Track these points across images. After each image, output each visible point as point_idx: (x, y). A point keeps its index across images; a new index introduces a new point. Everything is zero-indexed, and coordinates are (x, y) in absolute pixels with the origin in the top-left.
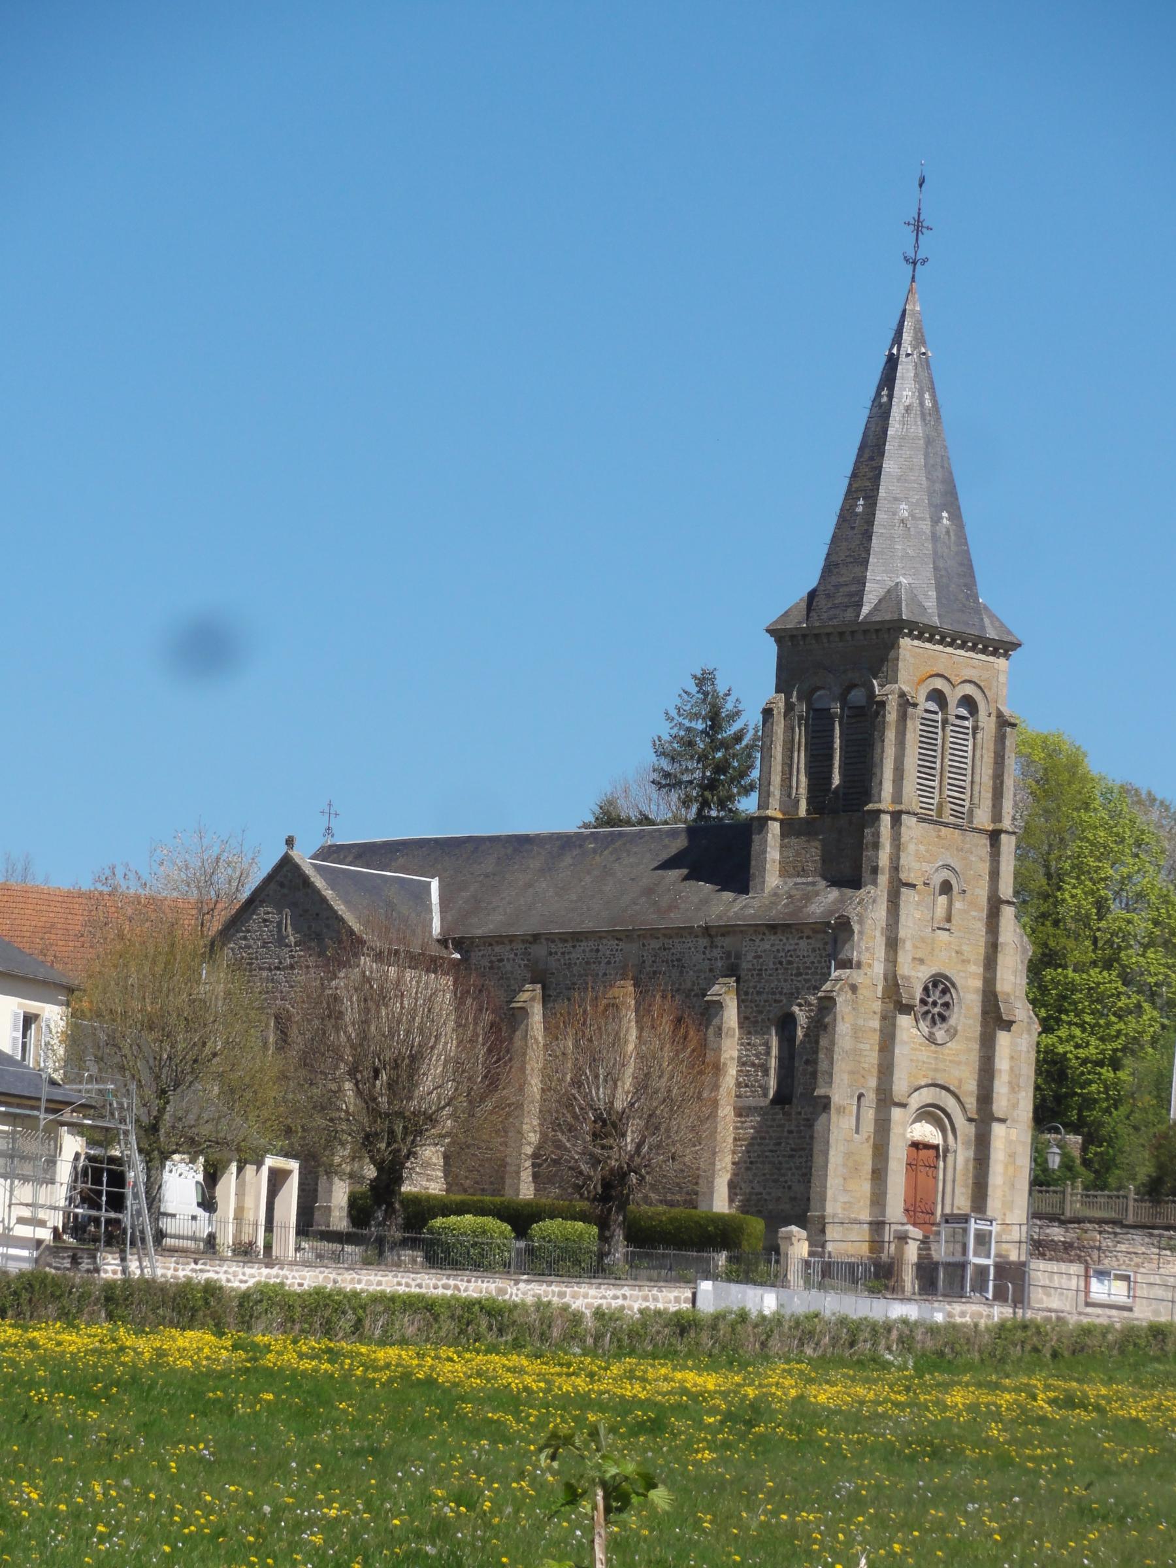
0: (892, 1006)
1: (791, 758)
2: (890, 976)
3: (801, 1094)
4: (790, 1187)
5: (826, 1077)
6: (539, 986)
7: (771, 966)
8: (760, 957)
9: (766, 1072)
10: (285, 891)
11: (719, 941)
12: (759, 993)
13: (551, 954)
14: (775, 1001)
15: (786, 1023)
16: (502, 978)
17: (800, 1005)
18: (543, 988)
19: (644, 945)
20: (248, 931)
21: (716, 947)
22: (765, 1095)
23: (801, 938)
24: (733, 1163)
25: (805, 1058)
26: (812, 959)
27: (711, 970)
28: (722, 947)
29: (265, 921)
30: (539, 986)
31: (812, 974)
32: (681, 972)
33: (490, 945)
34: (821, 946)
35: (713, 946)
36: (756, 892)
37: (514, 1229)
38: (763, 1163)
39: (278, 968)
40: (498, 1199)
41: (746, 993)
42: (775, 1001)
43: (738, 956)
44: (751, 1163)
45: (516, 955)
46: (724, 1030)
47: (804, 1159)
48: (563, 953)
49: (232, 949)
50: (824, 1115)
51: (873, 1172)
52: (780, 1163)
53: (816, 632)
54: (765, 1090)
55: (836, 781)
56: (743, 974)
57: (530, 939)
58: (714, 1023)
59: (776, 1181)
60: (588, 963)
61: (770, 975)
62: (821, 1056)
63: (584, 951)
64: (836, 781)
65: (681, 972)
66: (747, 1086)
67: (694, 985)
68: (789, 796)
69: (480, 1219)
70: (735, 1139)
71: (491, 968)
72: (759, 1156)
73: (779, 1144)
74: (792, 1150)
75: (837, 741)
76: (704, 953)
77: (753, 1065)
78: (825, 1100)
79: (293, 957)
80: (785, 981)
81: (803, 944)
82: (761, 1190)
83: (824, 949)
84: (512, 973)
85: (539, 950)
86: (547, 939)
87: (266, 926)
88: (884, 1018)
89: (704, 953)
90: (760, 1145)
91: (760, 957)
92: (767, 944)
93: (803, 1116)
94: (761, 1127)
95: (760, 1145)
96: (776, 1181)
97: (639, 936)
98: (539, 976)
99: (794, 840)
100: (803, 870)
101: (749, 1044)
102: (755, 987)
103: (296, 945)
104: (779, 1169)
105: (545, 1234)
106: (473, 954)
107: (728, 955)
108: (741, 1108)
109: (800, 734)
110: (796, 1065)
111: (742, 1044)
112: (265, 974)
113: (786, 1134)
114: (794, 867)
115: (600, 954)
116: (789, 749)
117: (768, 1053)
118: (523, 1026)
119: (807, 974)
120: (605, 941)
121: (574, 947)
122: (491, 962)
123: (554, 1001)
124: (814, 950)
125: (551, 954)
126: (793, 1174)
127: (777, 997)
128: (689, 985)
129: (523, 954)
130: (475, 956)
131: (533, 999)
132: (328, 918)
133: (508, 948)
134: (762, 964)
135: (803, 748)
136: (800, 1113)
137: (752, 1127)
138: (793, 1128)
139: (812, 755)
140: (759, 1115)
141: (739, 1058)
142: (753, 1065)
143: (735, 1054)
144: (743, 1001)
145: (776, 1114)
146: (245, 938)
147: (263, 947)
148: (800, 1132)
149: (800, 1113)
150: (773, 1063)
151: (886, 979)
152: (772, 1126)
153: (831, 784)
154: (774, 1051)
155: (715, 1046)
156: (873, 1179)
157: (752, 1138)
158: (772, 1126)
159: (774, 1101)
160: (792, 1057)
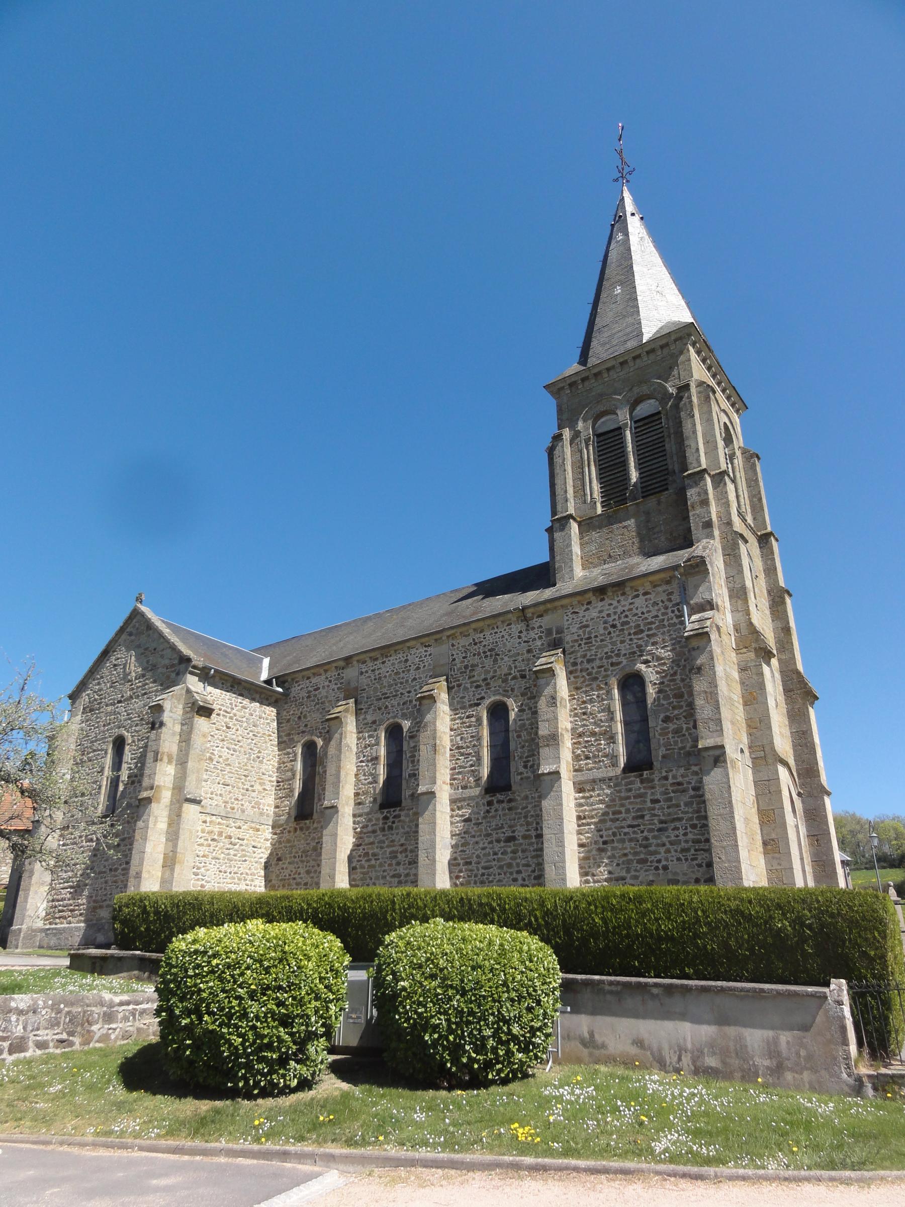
0: (752, 655)
1: (583, 473)
2: (743, 626)
3: (664, 757)
4: (665, 868)
5: (711, 725)
6: (353, 700)
7: (602, 631)
8: (587, 626)
9: (612, 739)
10: (133, 637)
11: (536, 622)
12: (589, 661)
13: (362, 673)
14: (612, 664)
15: (632, 684)
16: (318, 704)
17: (646, 662)
18: (356, 702)
19: (453, 645)
20: (102, 677)
21: (533, 628)
22: (615, 764)
23: (637, 596)
24: (581, 845)
25: (662, 716)
26: (654, 613)
27: (529, 651)
28: (541, 627)
29: (115, 665)
30: (353, 700)
31: (657, 628)
32: (495, 661)
33: (308, 678)
34: (665, 598)
35: (528, 628)
36: (563, 582)
37: (348, 948)
38: (622, 841)
39: (119, 702)
40: (313, 893)
41: (575, 664)
42: (612, 664)
43: (560, 631)
44: (605, 843)
45: (330, 681)
46: (559, 699)
47: (681, 832)
48: (373, 671)
49: (88, 695)
50: (717, 773)
51: (765, 844)
52: (646, 839)
53: (595, 371)
54: (614, 758)
55: (634, 475)
56: (567, 646)
57: (342, 664)
58: (546, 693)
59: (643, 861)
60: (397, 673)
61: (602, 641)
62: (699, 702)
63: (393, 664)
64: (634, 475)
65: (495, 661)
66: (587, 758)
67: (510, 668)
68: (585, 502)
69: (276, 929)
70: (579, 818)
71: (309, 697)
72: (614, 834)
73: (642, 817)
74: (661, 822)
75: (630, 448)
76: (520, 637)
77: (593, 734)
78: (717, 752)
79: (133, 689)
80: (622, 642)
81: (640, 602)
82: (624, 874)
83: (670, 600)
84: (327, 697)
85: (351, 673)
86: (358, 661)
87: (116, 670)
88: (743, 669)
89: (520, 637)
90: (612, 820)
91: (587, 626)
92: (595, 611)
93: (671, 781)
94: (613, 800)
95: (612, 820)
96: (643, 861)
97: (448, 637)
98: (351, 692)
99: (595, 535)
100: (610, 556)
101: (584, 714)
102: (584, 656)
103: (136, 679)
104: (646, 847)
105: (422, 956)
106: (293, 689)
107: (549, 632)
108: (581, 783)
109: (589, 453)
110: (651, 724)
111: (576, 715)
112: (109, 709)
113: (649, 804)
114: (598, 558)
115: (409, 663)
116: (579, 467)
117: (612, 719)
118: (337, 736)
119: (649, 629)
120: (413, 651)
121: (383, 663)
122: (309, 692)
123: (365, 712)
124: (655, 604)
125: (362, 673)
126: (668, 851)
127: (614, 660)
128: (505, 670)
129: (337, 679)
130: (295, 690)
131: (346, 711)
132: (163, 650)
133: (323, 677)
134: (590, 633)
135: (592, 463)
136: (666, 778)
137: (601, 802)
138: (658, 797)
139: (600, 469)
140: (609, 787)
141: (573, 729)
142: (593, 734)
143: (569, 726)
144: (571, 672)
145: (632, 783)
146: (99, 684)
147: (111, 687)
148: (670, 799)
149: (666, 778)
150: (619, 728)
151: (737, 630)
152: (628, 798)
153: (630, 479)
154: (619, 716)
155: (550, 716)
156: (766, 853)
157: (603, 814)
158: (628, 798)
159: (628, 769)
160: (645, 720)
